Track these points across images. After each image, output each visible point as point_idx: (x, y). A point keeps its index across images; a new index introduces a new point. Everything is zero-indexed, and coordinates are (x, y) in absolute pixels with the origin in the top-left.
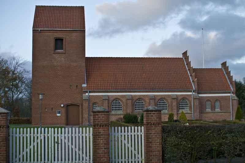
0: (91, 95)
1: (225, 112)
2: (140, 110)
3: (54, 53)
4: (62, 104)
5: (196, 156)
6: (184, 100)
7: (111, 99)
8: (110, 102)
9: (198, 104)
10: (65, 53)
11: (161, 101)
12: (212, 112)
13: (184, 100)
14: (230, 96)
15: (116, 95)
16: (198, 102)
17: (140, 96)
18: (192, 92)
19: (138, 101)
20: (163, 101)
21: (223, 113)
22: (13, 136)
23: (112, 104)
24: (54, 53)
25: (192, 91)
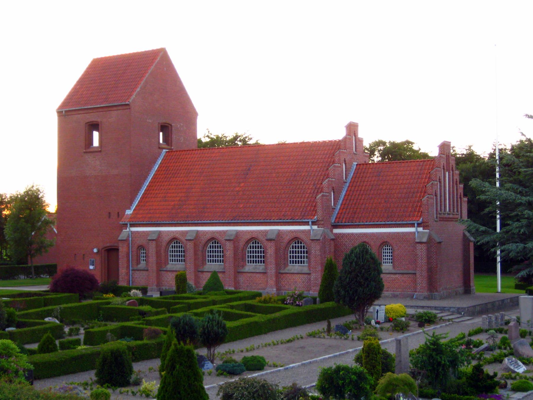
0: (134, 232)
1: (402, 272)
2: (256, 263)
3: (85, 152)
4: (96, 247)
5: (78, 321)
6: (256, 242)
7: (204, 239)
8: (164, 244)
9: (318, 253)
10: (100, 151)
11: (253, 243)
12: (394, 271)
13: (256, 242)
14: (414, 233)
15: (172, 232)
16: (318, 247)
17: (213, 232)
18: (309, 225)
19: (386, 247)
20: (301, 243)
21: (397, 276)
22: (254, 349)
23: (170, 249)
24: (85, 152)
25: (309, 222)
